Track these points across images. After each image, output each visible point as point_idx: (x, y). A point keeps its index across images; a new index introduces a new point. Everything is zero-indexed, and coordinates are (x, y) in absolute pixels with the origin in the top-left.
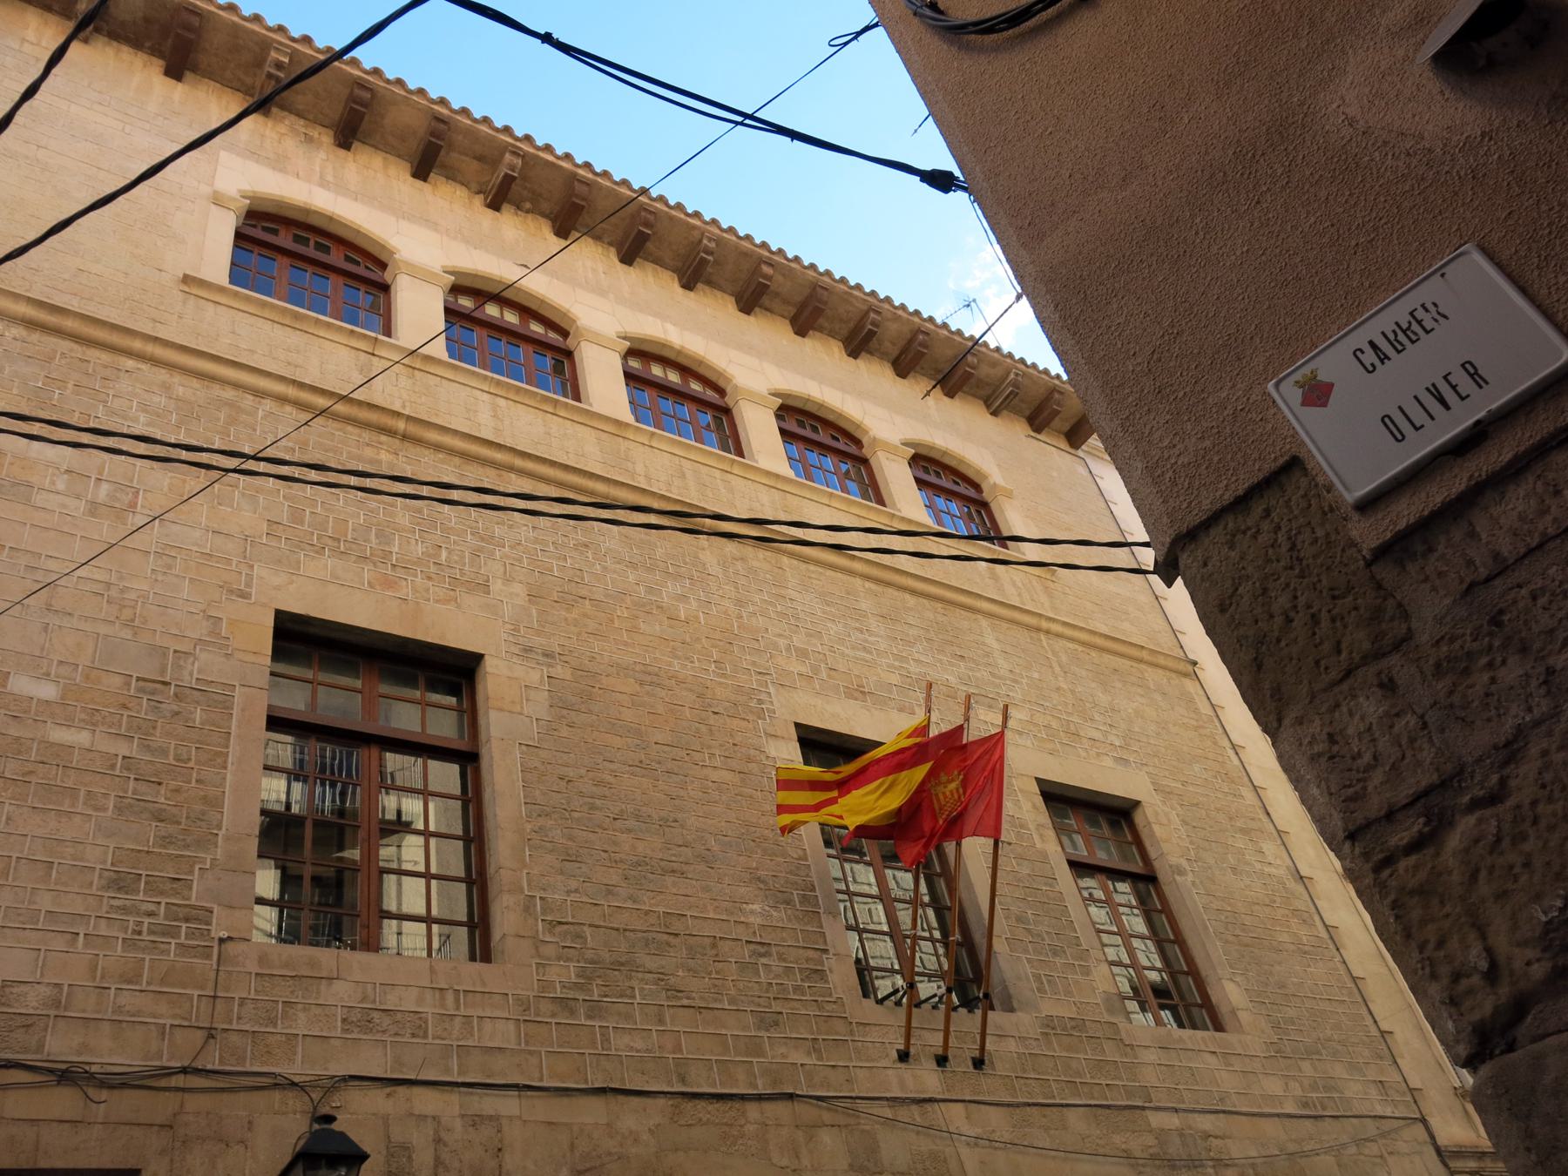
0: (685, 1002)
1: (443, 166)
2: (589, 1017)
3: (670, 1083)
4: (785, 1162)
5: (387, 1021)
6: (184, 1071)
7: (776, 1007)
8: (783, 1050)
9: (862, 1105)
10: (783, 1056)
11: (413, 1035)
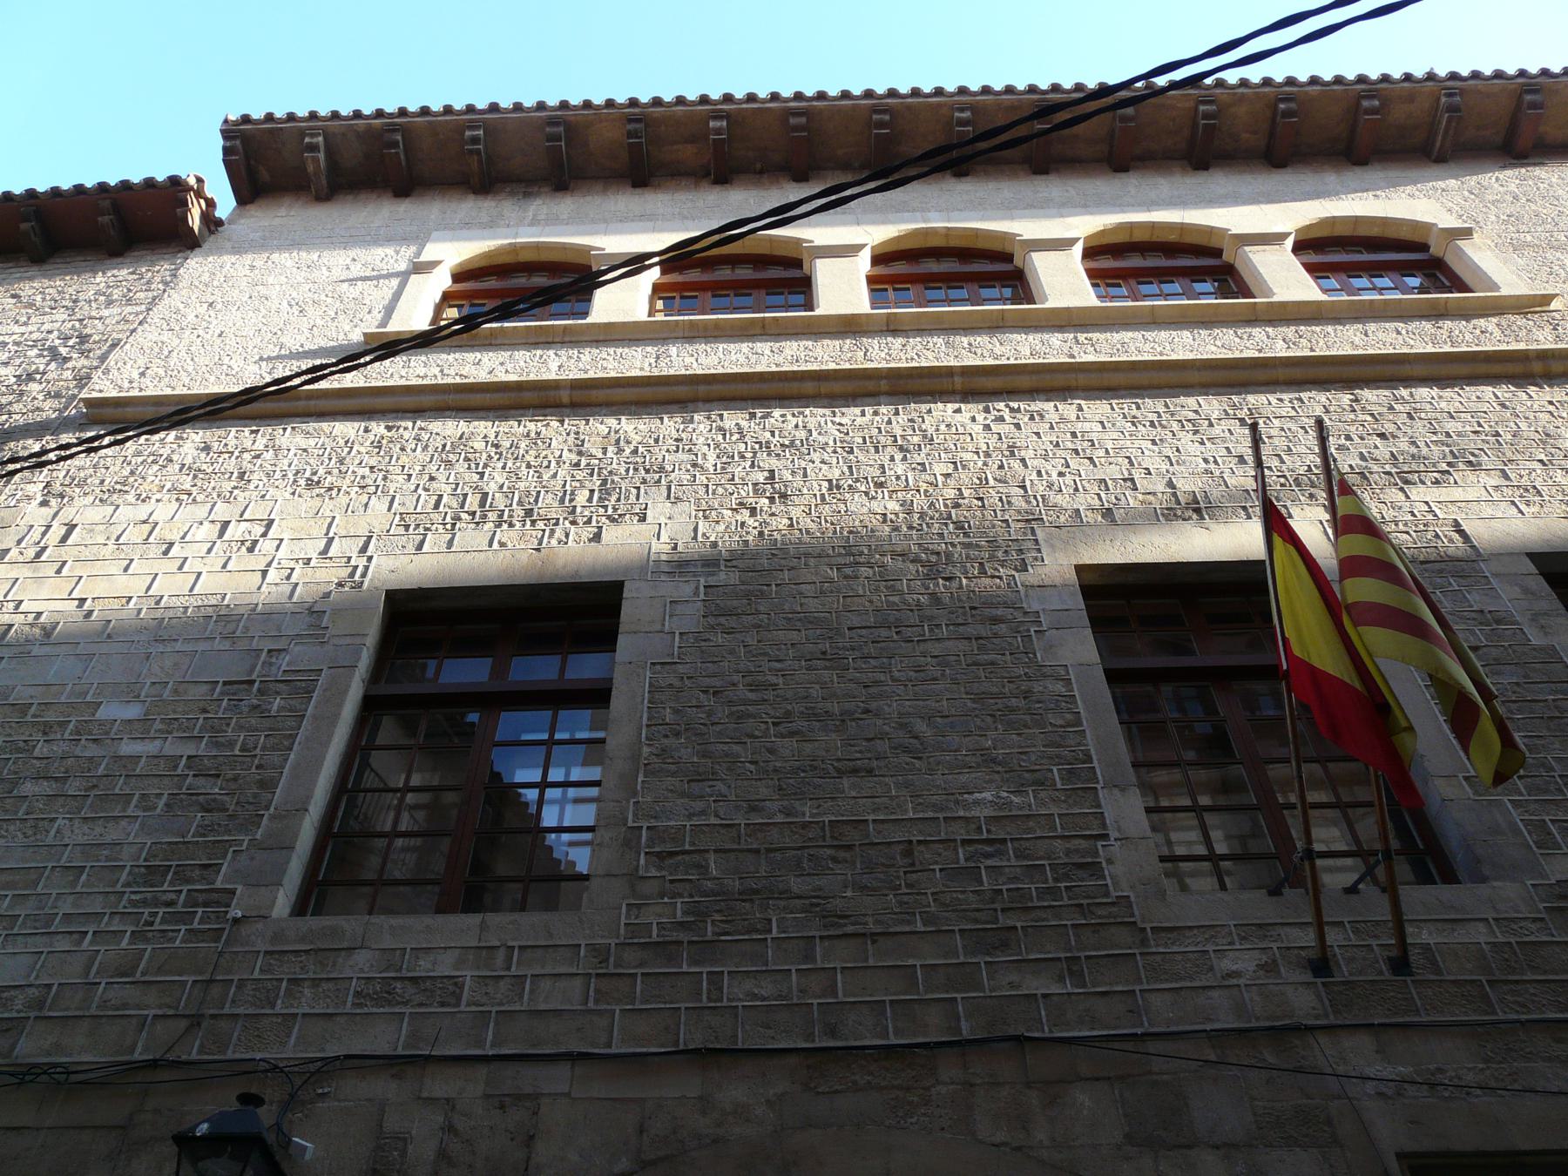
0: (850, 929)
2: (696, 963)
3: (810, 1037)
4: (1000, 1137)
5: (411, 989)
7: (1004, 921)
8: (1014, 977)
9: (1152, 1046)
10: (1012, 985)
11: (442, 1004)
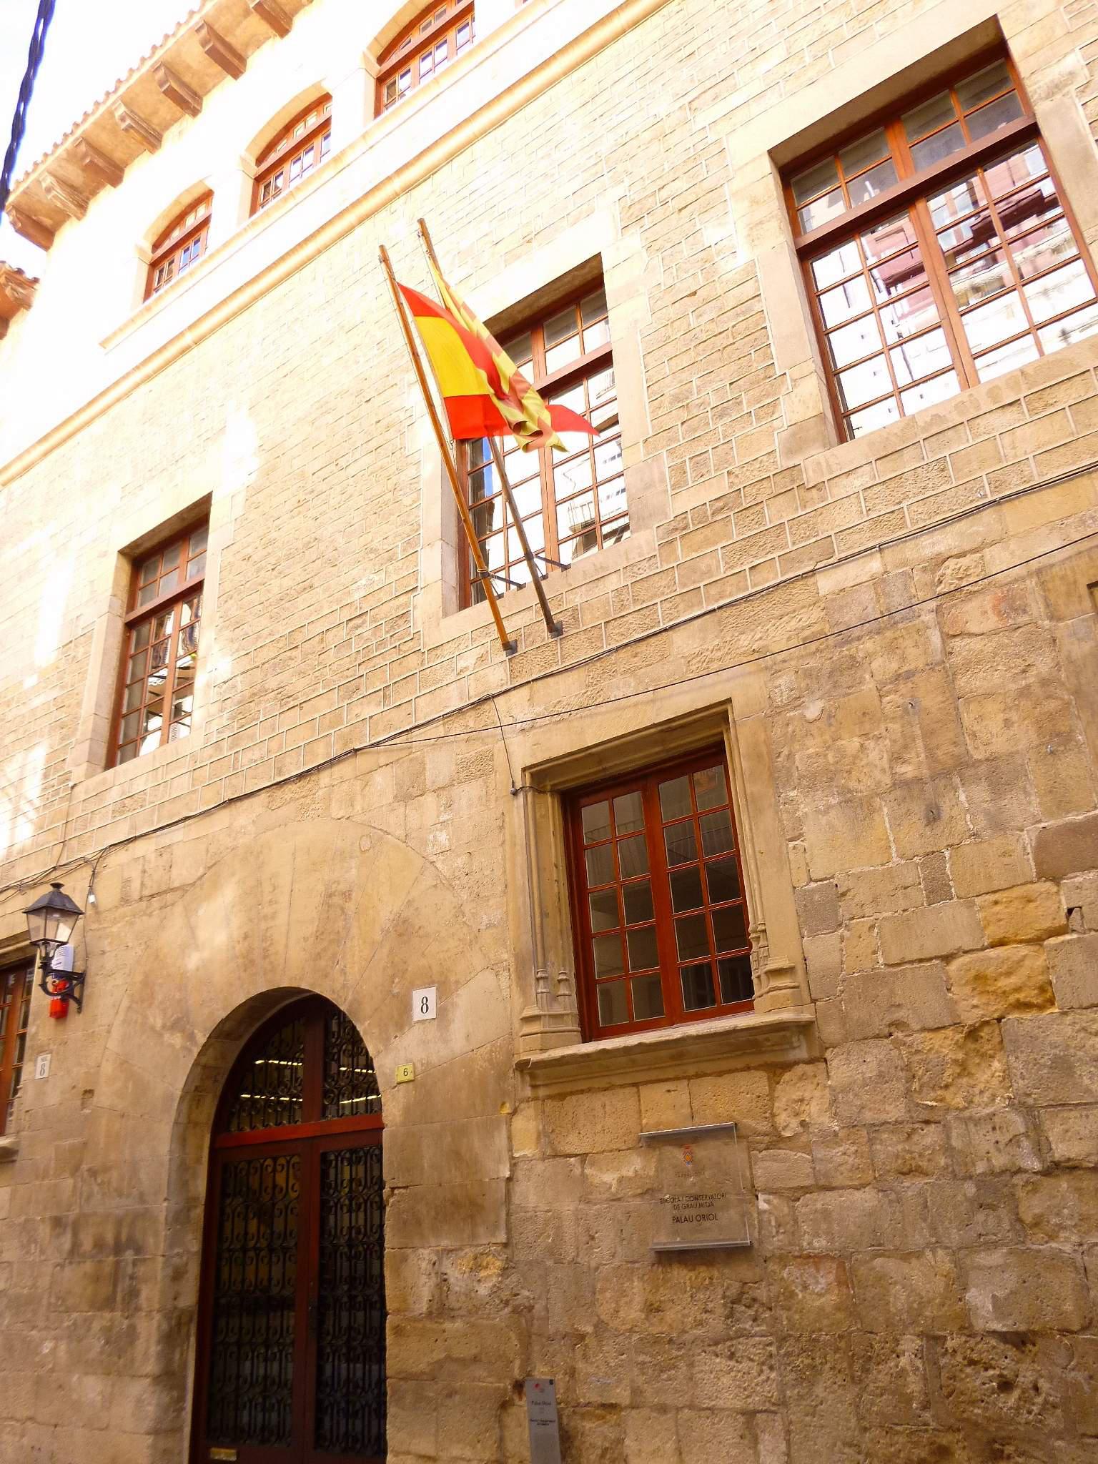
1: (247, 45)
6: (55, 868)
